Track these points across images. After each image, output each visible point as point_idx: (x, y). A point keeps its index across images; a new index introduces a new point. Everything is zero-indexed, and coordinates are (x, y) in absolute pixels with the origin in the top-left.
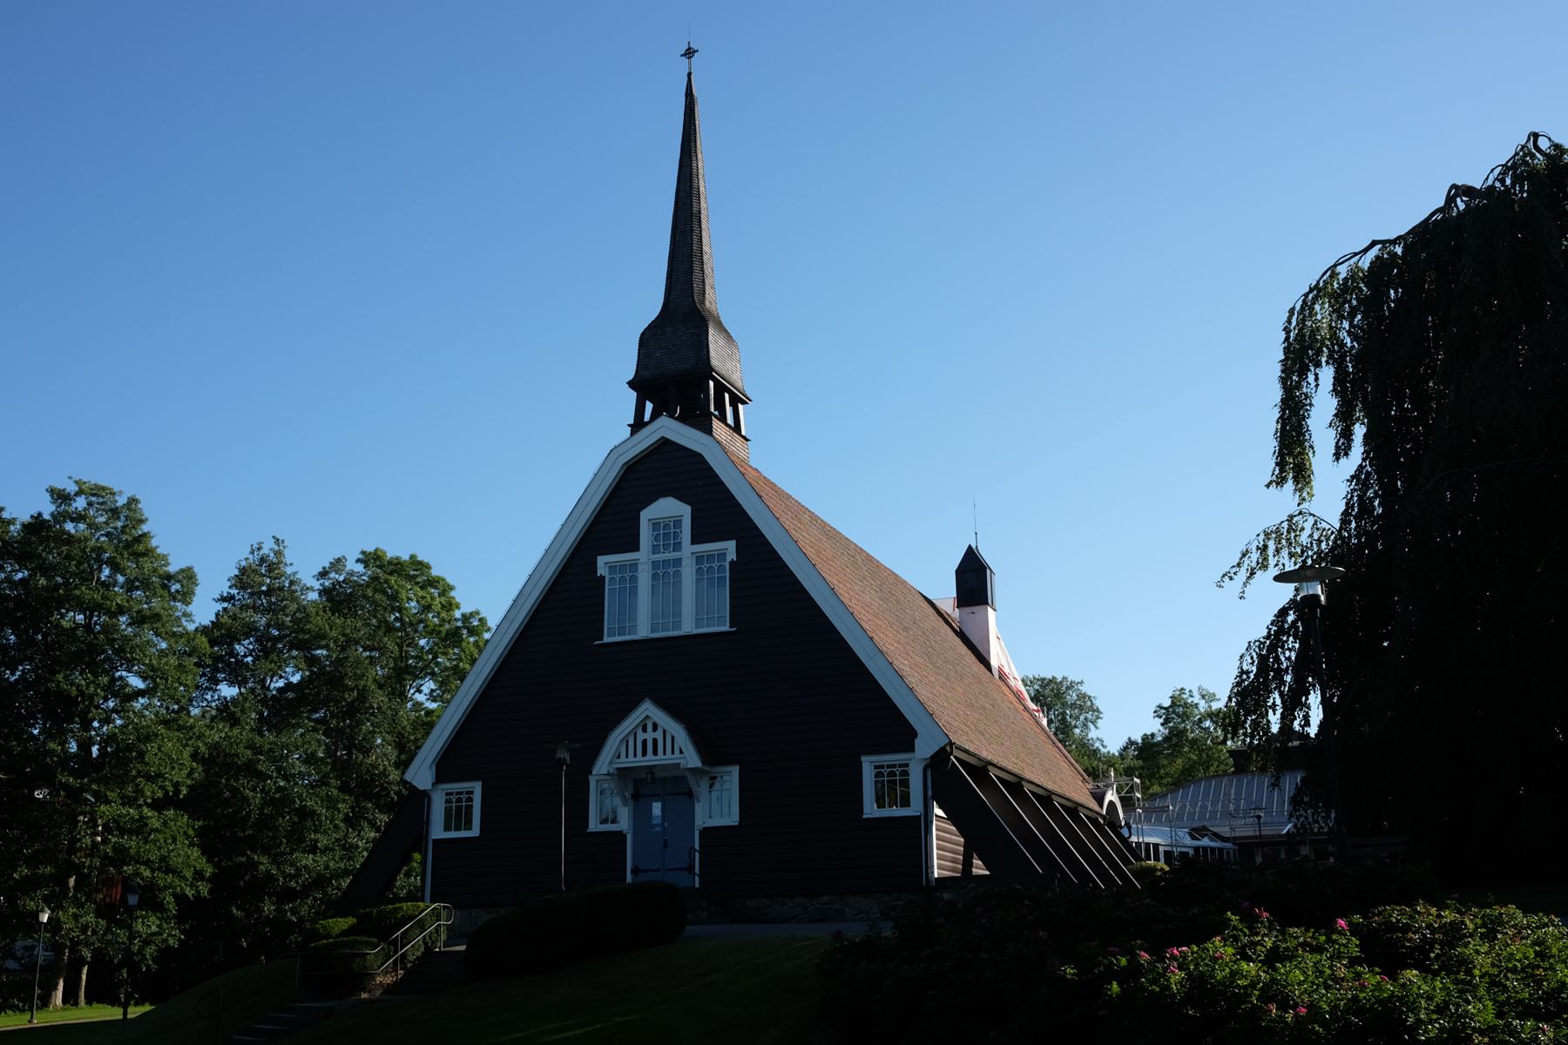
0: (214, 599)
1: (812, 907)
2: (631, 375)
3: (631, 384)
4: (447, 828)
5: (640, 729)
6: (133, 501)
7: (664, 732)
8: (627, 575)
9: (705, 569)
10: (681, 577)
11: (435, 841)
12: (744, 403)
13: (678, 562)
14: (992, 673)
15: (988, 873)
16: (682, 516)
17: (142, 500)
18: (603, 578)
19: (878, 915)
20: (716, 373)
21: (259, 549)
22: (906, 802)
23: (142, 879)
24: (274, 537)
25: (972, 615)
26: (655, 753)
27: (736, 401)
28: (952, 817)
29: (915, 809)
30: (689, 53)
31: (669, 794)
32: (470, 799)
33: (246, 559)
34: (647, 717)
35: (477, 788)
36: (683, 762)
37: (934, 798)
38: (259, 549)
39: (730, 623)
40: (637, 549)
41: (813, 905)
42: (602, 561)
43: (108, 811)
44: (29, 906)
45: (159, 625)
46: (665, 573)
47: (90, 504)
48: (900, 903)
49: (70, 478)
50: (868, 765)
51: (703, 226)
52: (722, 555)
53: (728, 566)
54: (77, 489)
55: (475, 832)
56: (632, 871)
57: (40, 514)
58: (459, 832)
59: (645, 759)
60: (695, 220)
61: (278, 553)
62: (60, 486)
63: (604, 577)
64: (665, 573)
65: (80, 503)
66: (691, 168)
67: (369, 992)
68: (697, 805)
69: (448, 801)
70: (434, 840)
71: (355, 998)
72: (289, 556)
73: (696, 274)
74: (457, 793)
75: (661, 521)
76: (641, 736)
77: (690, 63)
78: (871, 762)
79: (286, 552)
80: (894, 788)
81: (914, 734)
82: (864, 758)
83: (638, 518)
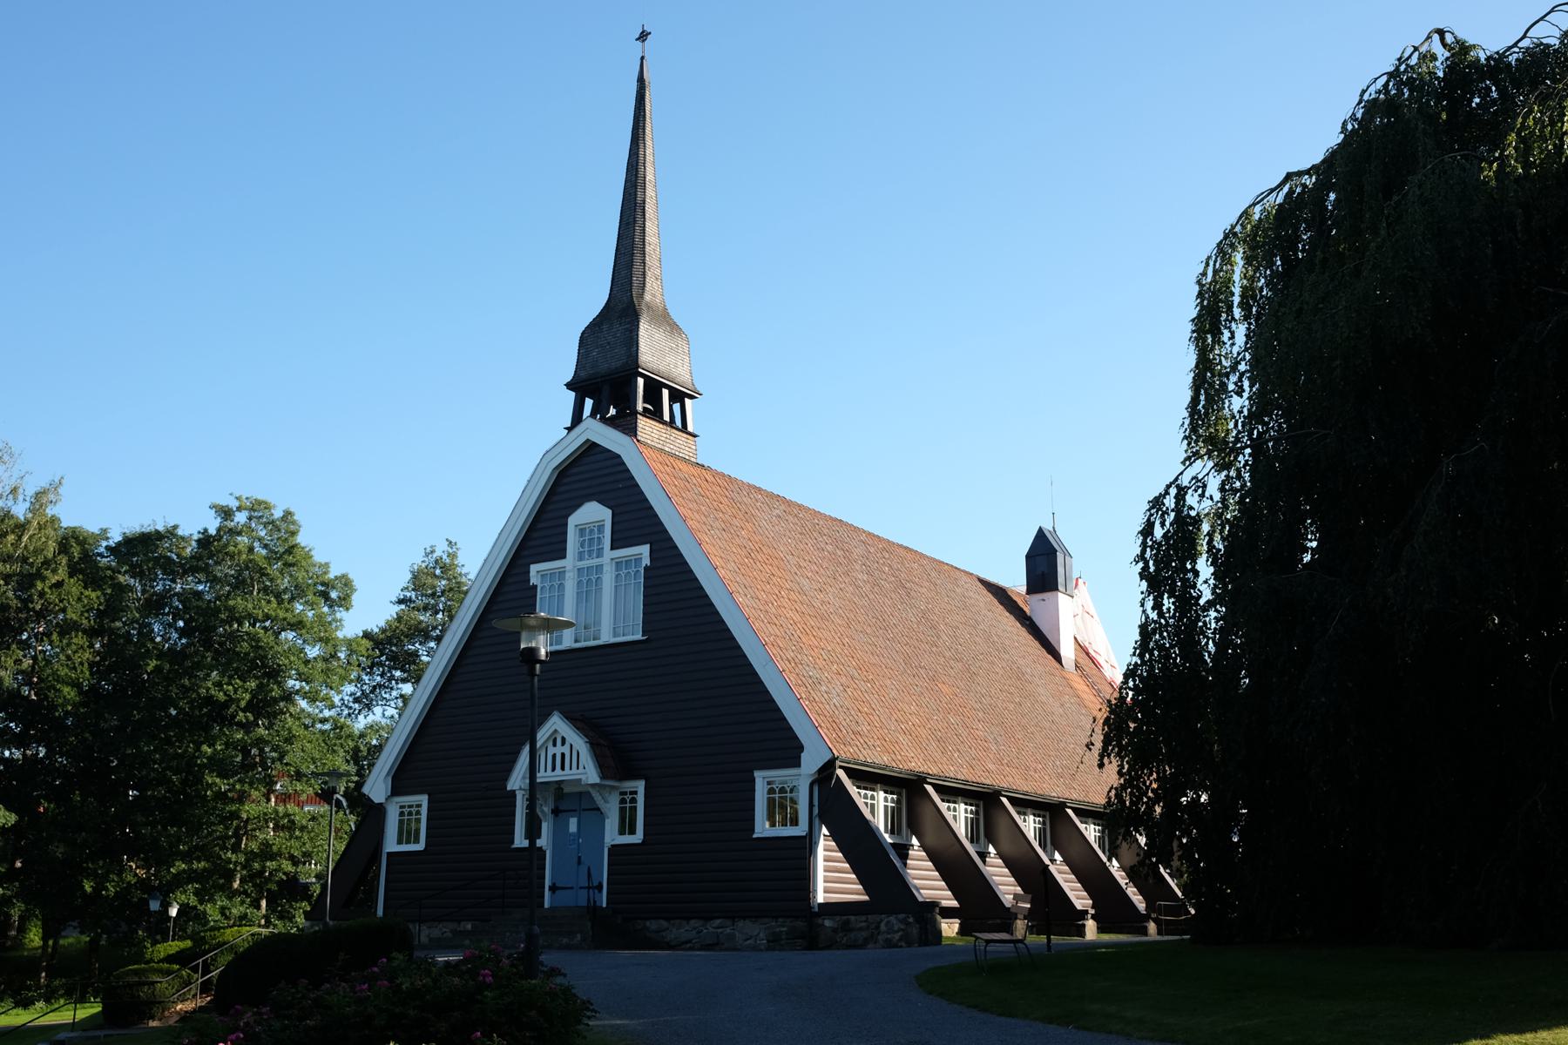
0: (391, 602)
1: (705, 931)
2: (569, 376)
3: (570, 386)
4: (400, 842)
5: (551, 743)
6: (288, 514)
7: (571, 746)
8: (594, 577)
9: (633, 574)
10: (602, 585)
11: (389, 854)
12: (692, 397)
13: (599, 568)
14: (1062, 665)
15: (866, 898)
16: (603, 521)
17: (296, 512)
18: (535, 587)
19: (765, 942)
20: (643, 369)
21: (432, 552)
22: (795, 822)
23: (285, 873)
24: (447, 540)
25: (1042, 602)
26: (563, 768)
27: (678, 396)
28: (834, 835)
29: (800, 830)
30: (643, 36)
31: (584, 810)
32: (418, 813)
33: (423, 562)
34: (556, 731)
35: (423, 800)
36: (583, 777)
37: (824, 821)
38: (432, 552)
39: (643, 631)
40: (564, 557)
41: (707, 929)
42: (534, 568)
43: (253, 810)
44: (180, 899)
45: (304, 631)
46: (589, 582)
47: (250, 519)
48: (785, 929)
49: (231, 494)
50: (761, 779)
51: (647, 215)
52: (638, 560)
53: (643, 571)
54: (237, 504)
55: (420, 846)
56: (550, 888)
57: (206, 530)
58: (409, 845)
59: (554, 774)
60: (639, 210)
61: (453, 556)
62: (223, 503)
63: (537, 586)
64: (589, 582)
65: (241, 518)
66: (638, 157)
67: (160, 1020)
68: (606, 821)
69: (402, 814)
70: (388, 854)
71: (143, 1026)
72: (460, 560)
73: (637, 266)
74: (410, 806)
75: (587, 526)
76: (551, 751)
77: (643, 47)
78: (764, 778)
79: (459, 554)
80: (781, 807)
81: (801, 748)
82: (757, 774)
83: (566, 525)
